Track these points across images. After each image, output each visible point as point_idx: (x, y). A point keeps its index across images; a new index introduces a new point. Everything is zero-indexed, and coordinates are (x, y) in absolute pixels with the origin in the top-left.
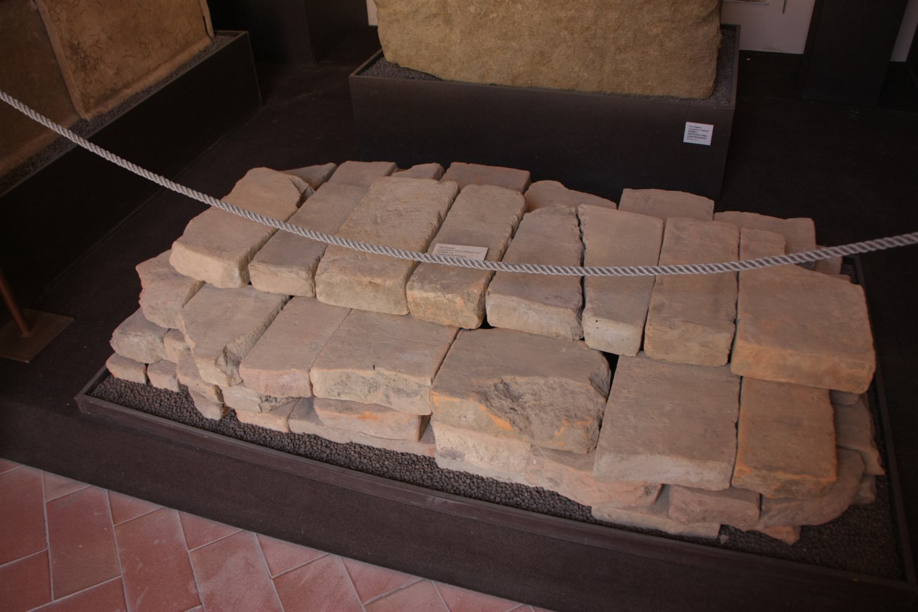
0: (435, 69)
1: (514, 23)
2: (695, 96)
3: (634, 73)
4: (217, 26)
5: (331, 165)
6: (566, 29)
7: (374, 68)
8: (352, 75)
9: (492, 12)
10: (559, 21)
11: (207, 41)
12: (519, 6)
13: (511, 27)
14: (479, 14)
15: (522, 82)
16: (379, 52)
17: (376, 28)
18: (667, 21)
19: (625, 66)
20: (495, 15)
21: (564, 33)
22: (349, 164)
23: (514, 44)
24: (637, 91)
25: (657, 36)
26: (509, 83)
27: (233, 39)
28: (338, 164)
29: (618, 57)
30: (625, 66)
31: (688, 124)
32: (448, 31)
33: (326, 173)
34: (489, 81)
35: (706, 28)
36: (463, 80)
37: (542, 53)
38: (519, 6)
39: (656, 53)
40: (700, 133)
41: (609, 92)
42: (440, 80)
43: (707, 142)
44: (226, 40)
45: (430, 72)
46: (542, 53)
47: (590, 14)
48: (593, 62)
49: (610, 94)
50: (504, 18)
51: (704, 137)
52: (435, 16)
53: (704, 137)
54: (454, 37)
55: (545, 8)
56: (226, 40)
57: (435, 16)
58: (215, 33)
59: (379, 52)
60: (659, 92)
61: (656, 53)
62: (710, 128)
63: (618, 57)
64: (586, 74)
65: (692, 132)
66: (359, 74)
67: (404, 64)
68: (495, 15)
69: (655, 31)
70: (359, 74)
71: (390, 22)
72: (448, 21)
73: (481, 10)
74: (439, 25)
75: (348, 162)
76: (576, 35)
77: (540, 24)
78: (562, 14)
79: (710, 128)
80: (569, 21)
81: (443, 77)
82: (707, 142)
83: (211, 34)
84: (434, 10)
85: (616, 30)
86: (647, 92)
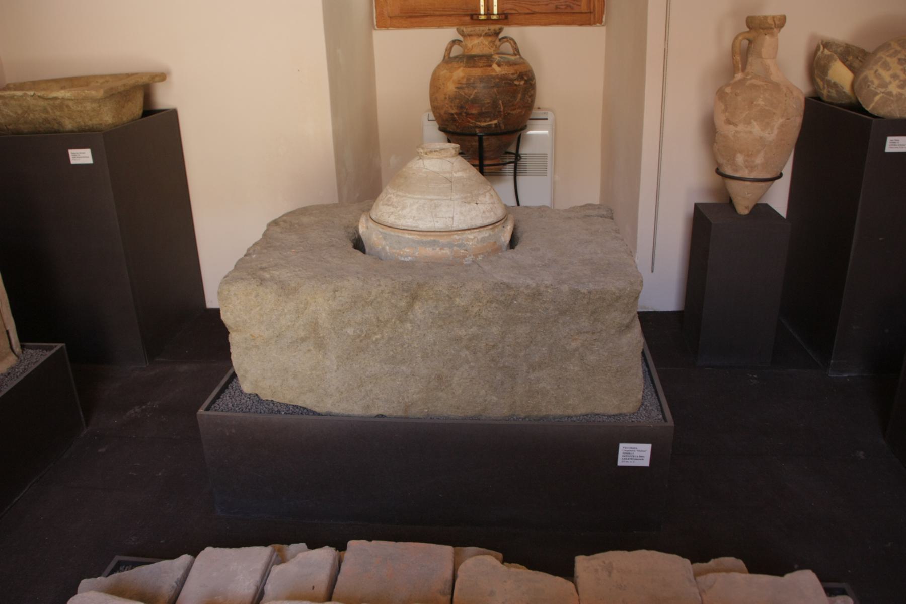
0: (307, 401)
1: (402, 345)
2: (624, 411)
3: (552, 392)
4: (25, 336)
5: (185, 558)
6: (468, 348)
7: (226, 397)
8: (201, 411)
9: (375, 333)
10: (458, 340)
11: (12, 360)
12: (408, 325)
13: (399, 349)
14: (359, 336)
15: (417, 412)
16: (231, 372)
17: (217, 312)
18: (587, 332)
19: (541, 385)
20: (378, 336)
21: (464, 353)
22: (209, 552)
23: (404, 368)
24: (557, 411)
25: (576, 350)
26: (400, 413)
27: (49, 354)
28: (195, 553)
29: (532, 376)
30: (541, 385)
31: (622, 446)
32: (321, 357)
33: (179, 574)
34: (375, 412)
35: (629, 335)
36: (342, 412)
37: (439, 378)
38: (408, 325)
39: (577, 369)
40: (636, 453)
41: (523, 415)
42: (314, 413)
43: (646, 462)
44: (38, 356)
45: (300, 404)
46: (439, 378)
47: (495, 330)
48: (502, 383)
49: (524, 419)
50: (390, 339)
51: (642, 458)
52: (303, 340)
53: (642, 458)
54: (328, 363)
55: (440, 326)
56: (38, 356)
57: (303, 340)
58: (22, 347)
59: (231, 372)
60: (582, 410)
61: (577, 369)
62: (647, 448)
63: (532, 376)
64: (494, 398)
65: (627, 454)
66: (208, 409)
67: (266, 395)
68: (378, 336)
69: (574, 345)
70: (208, 409)
71: (246, 348)
72: (320, 345)
73: (362, 331)
74: (309, 351)
75: (209, 549)
76: (479, 355)
77: (435, 344)
78: (462, 332)
79: (647, 448)
80: (470, 340)
81: (317, 410)
82: (646, 462)
83: (17, 349)
84: (302, 334)
85: (527, 347)
86: (570, 412)
